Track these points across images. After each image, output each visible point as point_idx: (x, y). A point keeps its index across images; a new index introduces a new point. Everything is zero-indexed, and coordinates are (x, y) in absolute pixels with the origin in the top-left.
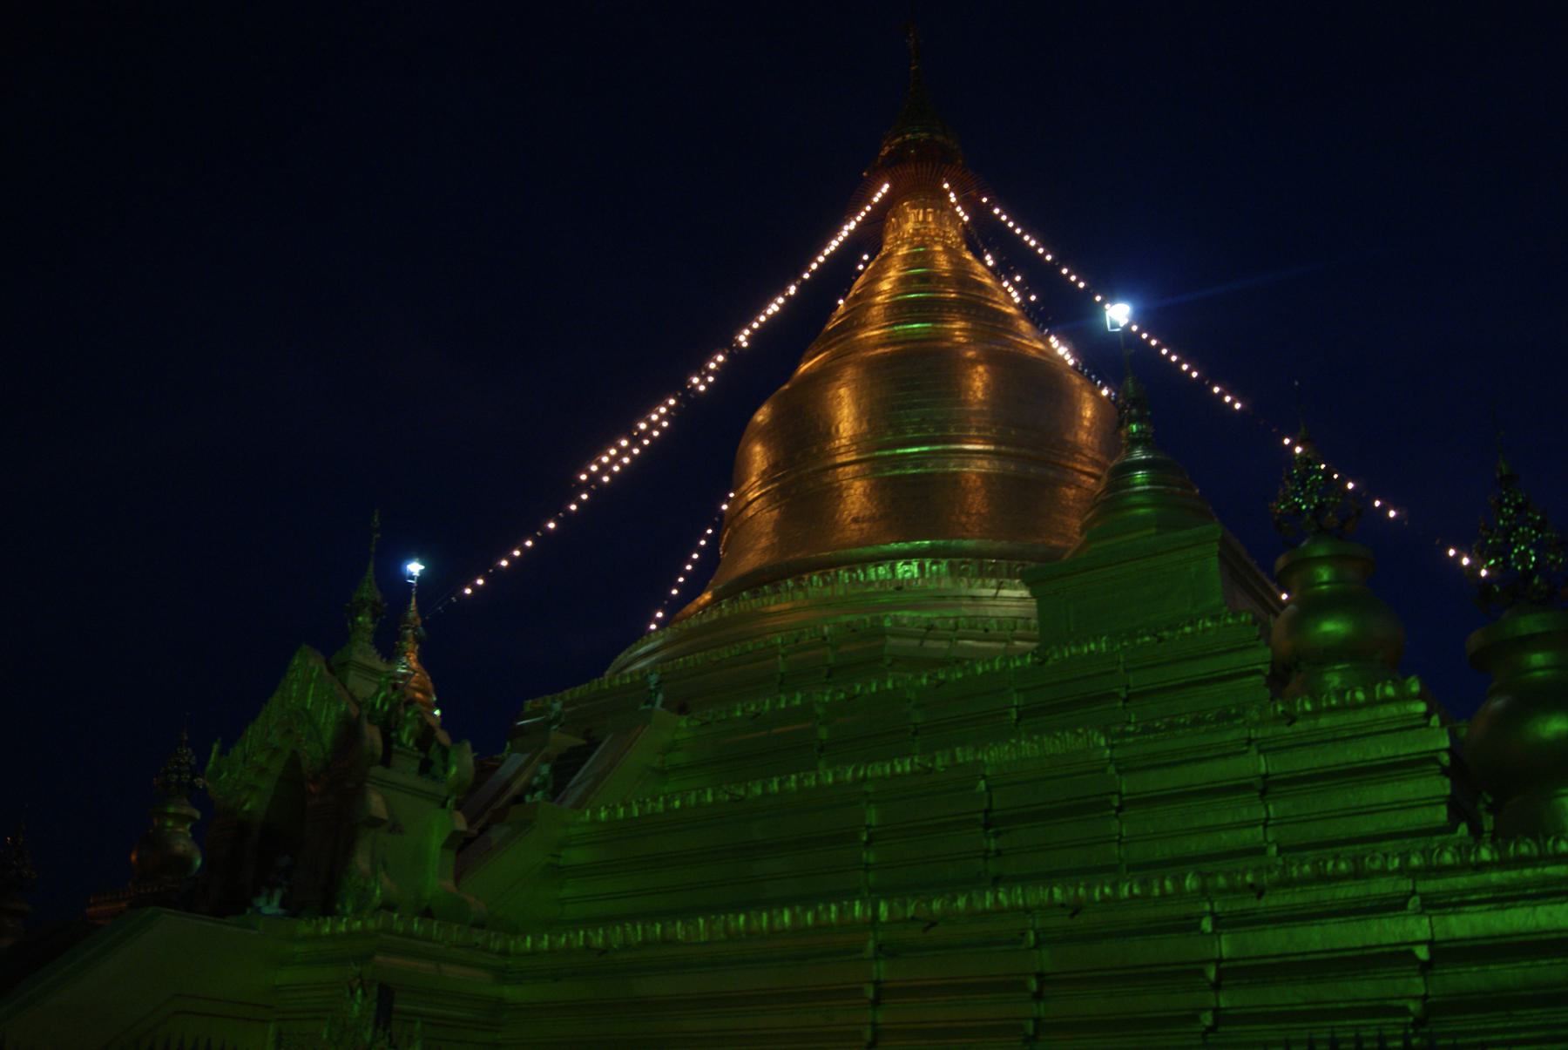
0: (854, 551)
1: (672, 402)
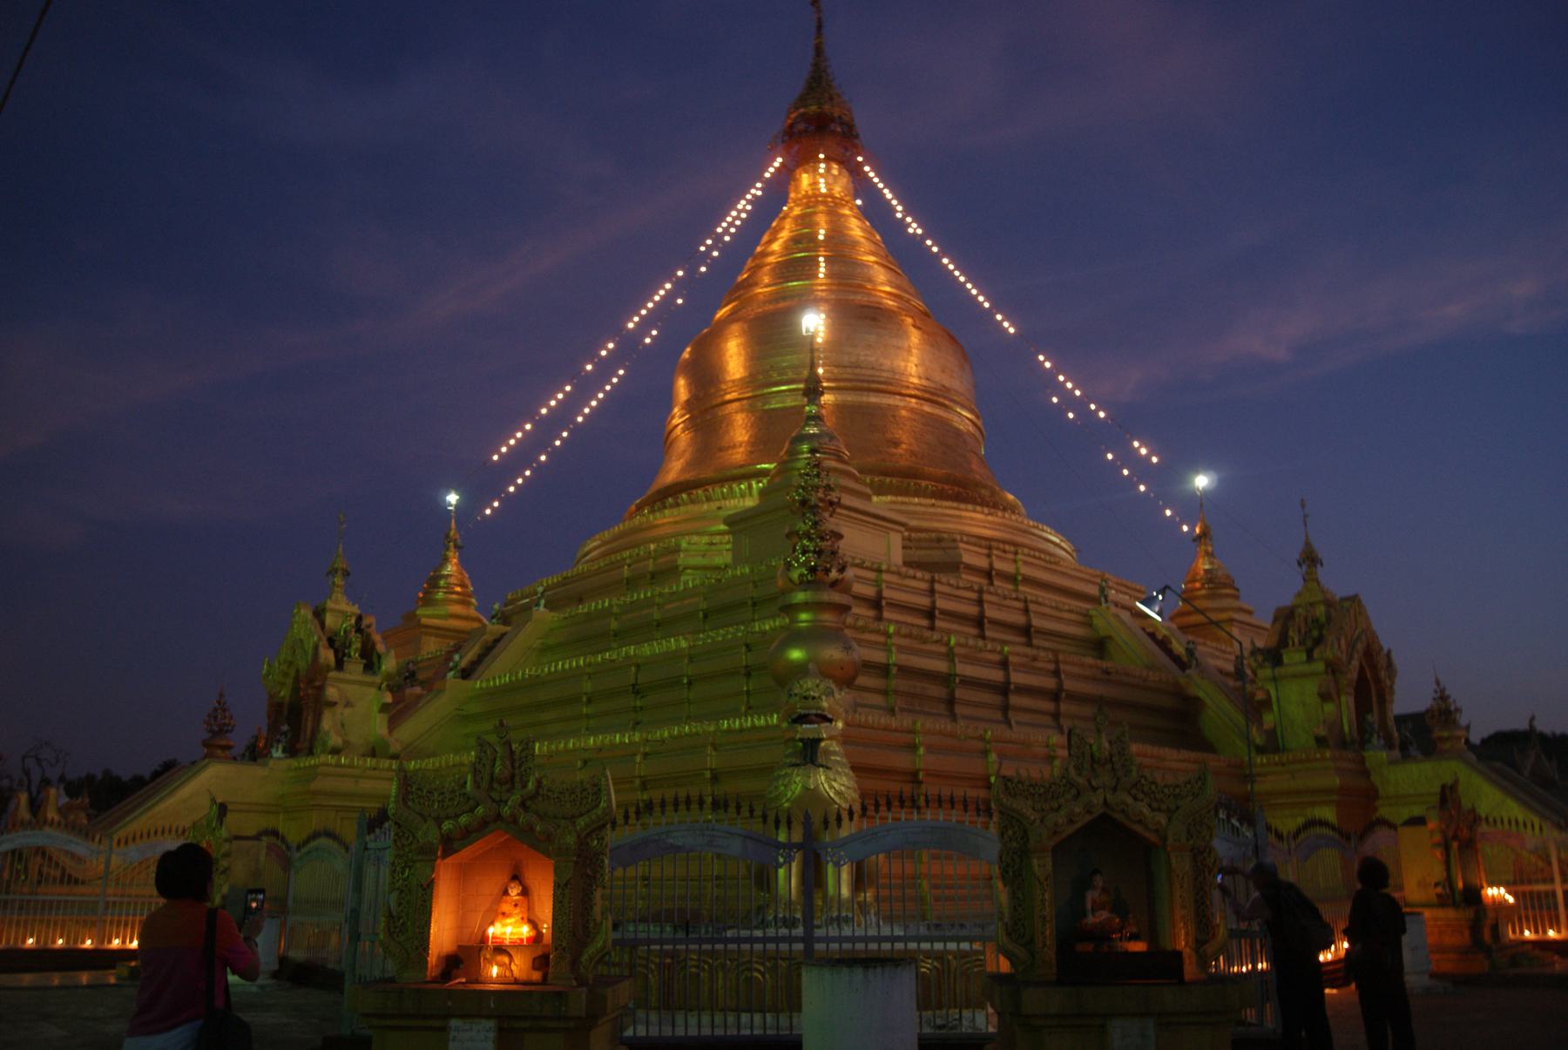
1: (654, 333)
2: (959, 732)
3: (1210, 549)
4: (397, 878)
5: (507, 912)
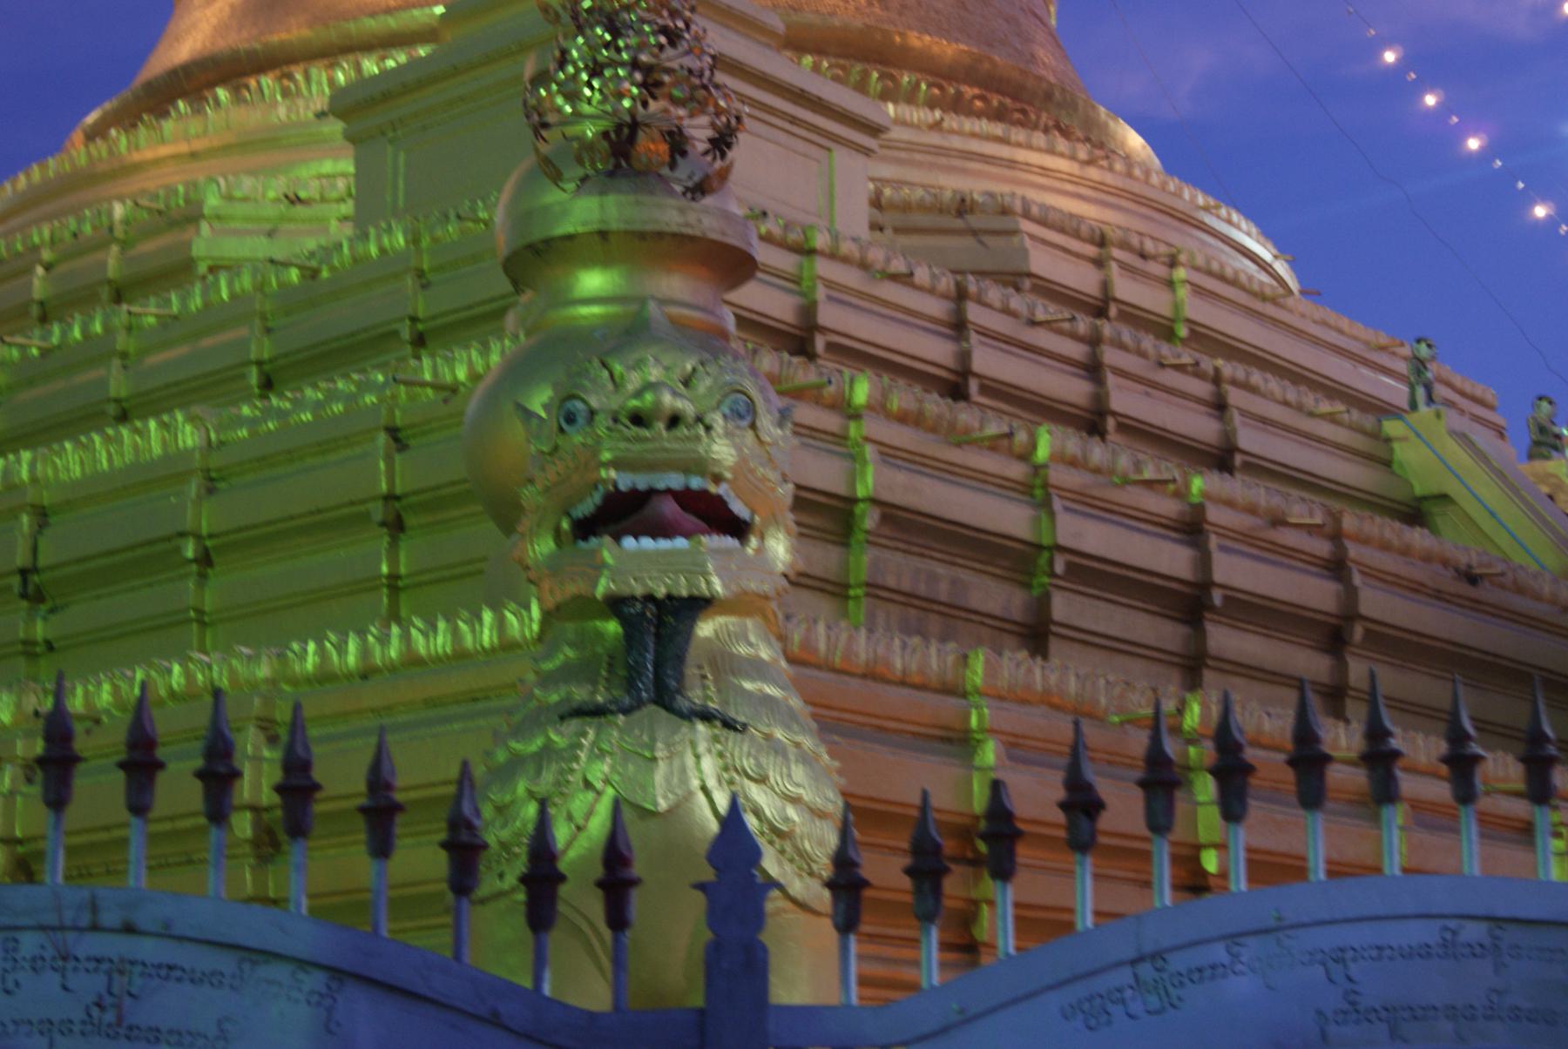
2: (1103, 701)
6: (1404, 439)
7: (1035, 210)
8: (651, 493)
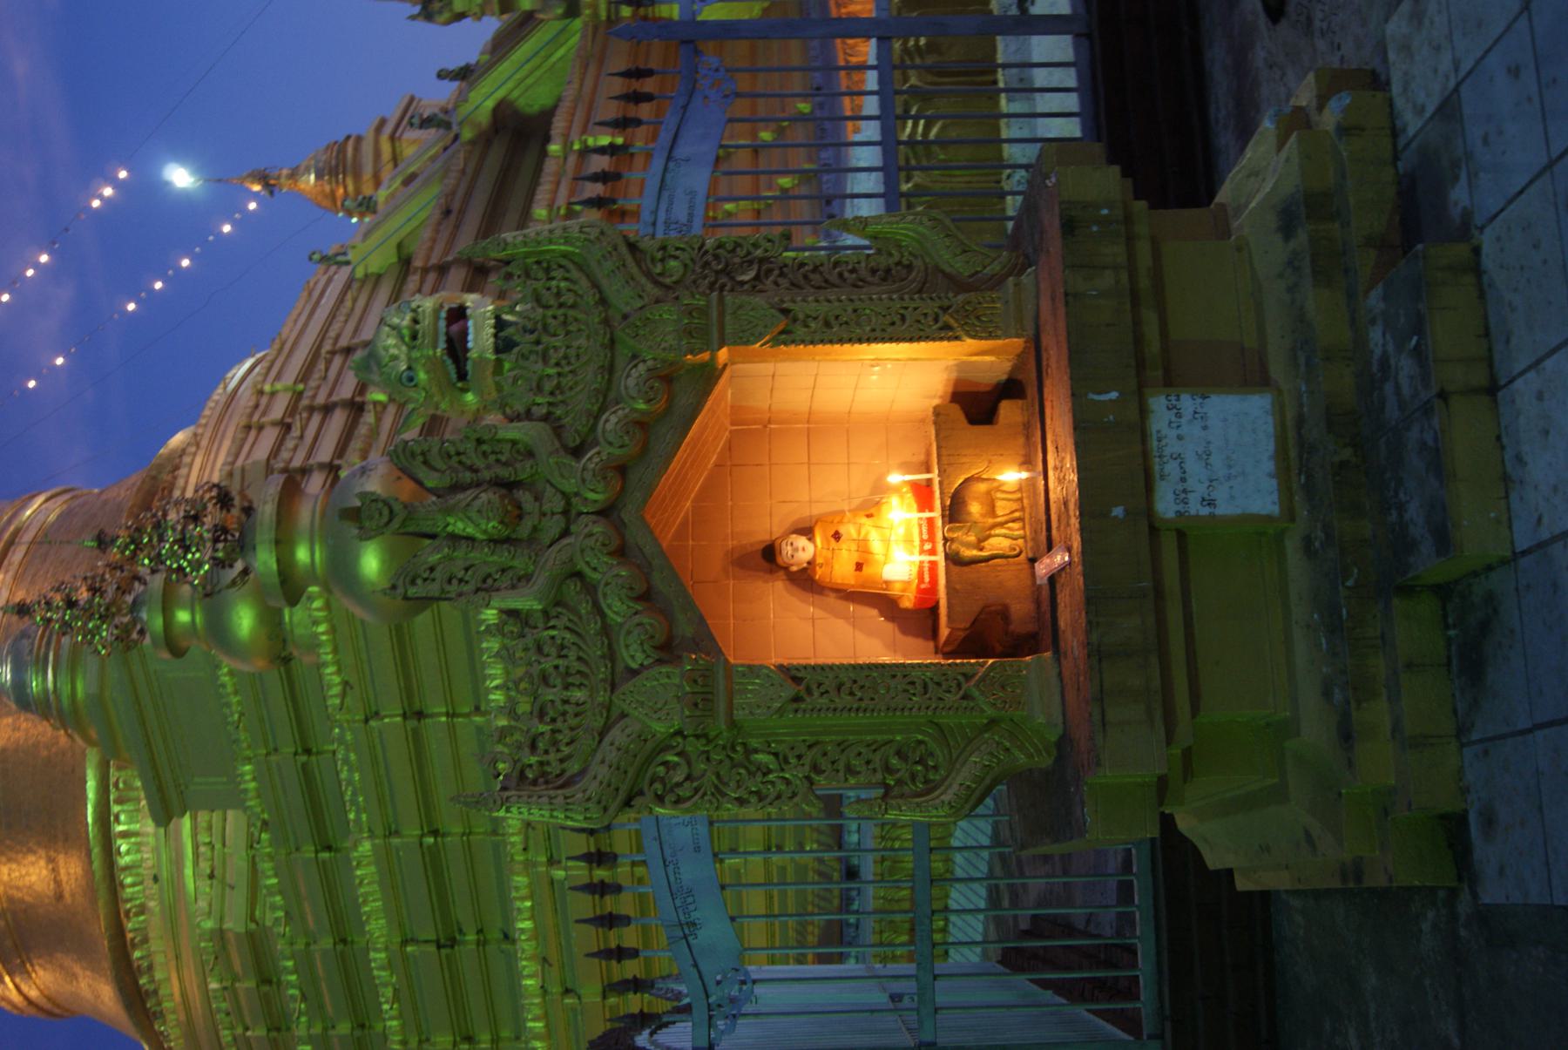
0: (97, 865)
3: (285, 172)
4: (782, 787)
5: (855, 557)
6: (366, 267)
7: (230, 459)
8: (447, 334)
